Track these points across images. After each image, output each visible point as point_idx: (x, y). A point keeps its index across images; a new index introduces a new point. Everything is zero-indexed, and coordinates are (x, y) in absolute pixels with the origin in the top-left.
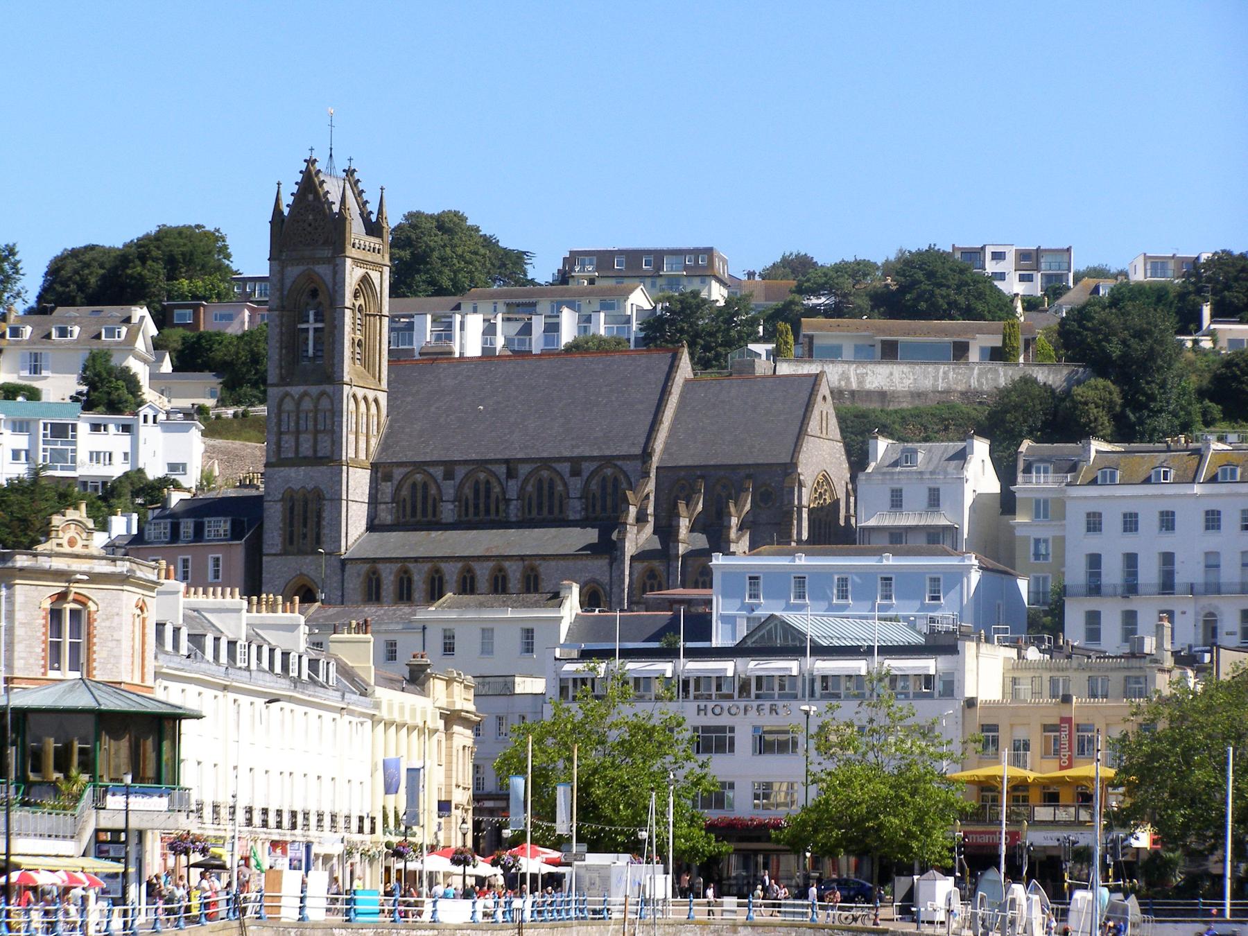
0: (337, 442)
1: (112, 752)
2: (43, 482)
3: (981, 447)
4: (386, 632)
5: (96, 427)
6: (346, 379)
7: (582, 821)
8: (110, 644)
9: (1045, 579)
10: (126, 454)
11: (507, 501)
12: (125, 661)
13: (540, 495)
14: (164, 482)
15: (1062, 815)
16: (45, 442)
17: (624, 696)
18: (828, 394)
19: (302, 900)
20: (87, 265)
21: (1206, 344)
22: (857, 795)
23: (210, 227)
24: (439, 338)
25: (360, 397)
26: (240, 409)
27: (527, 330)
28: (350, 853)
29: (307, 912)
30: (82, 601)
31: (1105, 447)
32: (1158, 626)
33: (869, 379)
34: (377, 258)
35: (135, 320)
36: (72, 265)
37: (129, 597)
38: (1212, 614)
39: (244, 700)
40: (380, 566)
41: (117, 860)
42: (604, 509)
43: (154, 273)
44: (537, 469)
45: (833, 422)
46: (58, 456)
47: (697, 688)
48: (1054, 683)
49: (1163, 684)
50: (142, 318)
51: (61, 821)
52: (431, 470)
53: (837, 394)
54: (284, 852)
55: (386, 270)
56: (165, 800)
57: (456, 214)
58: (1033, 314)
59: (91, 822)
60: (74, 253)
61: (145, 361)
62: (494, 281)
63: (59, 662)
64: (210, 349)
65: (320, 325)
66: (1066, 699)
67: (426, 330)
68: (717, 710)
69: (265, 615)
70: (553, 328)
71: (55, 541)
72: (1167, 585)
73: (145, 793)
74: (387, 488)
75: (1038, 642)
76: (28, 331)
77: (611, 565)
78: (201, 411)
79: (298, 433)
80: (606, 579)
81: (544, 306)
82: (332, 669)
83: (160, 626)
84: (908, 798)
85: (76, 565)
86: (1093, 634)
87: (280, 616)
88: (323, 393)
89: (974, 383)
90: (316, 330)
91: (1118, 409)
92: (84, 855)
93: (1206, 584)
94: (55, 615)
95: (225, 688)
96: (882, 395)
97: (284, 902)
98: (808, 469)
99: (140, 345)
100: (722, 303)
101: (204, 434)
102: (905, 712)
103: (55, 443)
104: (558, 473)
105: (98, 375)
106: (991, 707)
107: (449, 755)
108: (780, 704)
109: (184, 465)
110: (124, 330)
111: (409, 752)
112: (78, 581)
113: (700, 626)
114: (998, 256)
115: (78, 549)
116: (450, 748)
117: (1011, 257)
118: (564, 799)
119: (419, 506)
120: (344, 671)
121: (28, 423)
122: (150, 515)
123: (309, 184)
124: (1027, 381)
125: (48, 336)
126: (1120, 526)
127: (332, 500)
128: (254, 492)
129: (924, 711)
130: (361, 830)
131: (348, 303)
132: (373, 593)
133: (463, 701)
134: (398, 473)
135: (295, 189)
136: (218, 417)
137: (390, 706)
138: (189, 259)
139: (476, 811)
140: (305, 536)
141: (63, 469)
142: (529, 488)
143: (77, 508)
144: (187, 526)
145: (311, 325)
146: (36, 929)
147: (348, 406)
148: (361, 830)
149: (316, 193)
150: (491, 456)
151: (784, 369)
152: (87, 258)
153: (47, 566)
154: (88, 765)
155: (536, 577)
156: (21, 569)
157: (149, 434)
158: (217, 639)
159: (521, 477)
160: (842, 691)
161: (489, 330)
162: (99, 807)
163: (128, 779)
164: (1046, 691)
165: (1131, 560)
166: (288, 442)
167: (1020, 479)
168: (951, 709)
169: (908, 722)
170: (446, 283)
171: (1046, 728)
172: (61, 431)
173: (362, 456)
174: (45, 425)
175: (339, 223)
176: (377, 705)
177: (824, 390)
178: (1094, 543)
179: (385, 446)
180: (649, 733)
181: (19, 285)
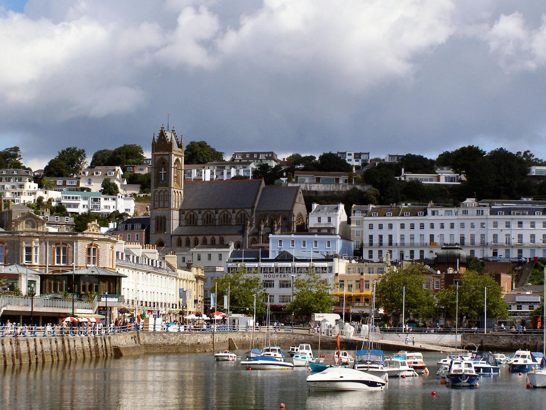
0: (170, 204)
1: (104, 286)
2: (91, 214)
3: (342, 207)
4: (182, 255)
5: (106, 199)
6: (172, 187)
7: (232, 305)
8: (104, 257)
9: (359, 241)
10: (114, 206)
11: (216, 220)
12: (108, 262)
13: (241, 217)
14: (124, 214)
15: (361, 305)
16: (92, 203)
17: (244, 272)
18: (301, 191)
19: (154, 325)
20: (104, 155)
21: (403, 179)
22: (305, 299)
23: (138, 145)
24: (198, 176)
25: (176, 191)
26: (145, 194)
27: (222, 174)
28: (170, 314)
29: (156, 329)
30: (96, 246)
31: (374, 207)
32: (387, 254)
33: (312, 188)
34: (181, 154)
35: (116, 170)
36: (100, 154)
37: (109, 245)
38: (402, 251)
39: (141, 273)
40: (181, 237)
41: (104, 315)
42: (241, 222)
43: (122, 157)
44: (224, 211)
45: (303, 199)
46: (95, 207)
47: (264, 270)
48: (359, 269)
49: (387, 270)
50: (119, 169)
51: (87, 305)
52: (195, 211)
53: (304, 191)
54: (152, 313)
55: (183, 157)
56: (117, 299)
57: (204, 142)
58: (358, 171)
59: (97, 305)
60: (101, 152)
61: (119, 181)
62: (214, 160)
63: (90, 262)
64: (137, 178)
65: (165, 172)
66: (362, 274)
67: (194, 174)
68: (269, 276)
69: (147, 250)
70: (229, 173)
71: (89, 230)
72: (390, 244)
73: (112, 297)
74: (184, 216)
75: (354, 258)
76: (87, 173)
77: (243, 237)
78: (135, 195)
79: (159, 201)
80: (242, 241)
81: (227, 167)
82: (165, 264)
83: (118, 253)
84: (319, 300)
85: (94, 236)
86: (371, 257)
87: (151, 250)
88: (166, 191)
89: (340, 189)
90: (164, 173)
91: (379, 196)
92: (95, 313)
93: (411, 243)
94: (89, 250)
95: (135, 269)
96: (316, 192)
97: (149, 326)
98: (296, 212)
99: (118, 177)
100: (274, 167)
101: (135, 201)
102: (318, 277)
103: (95, 203)
104: (212, 212)
105: (107, 185)
106: (342, 276)
107: (197, 288)
108: (286, 274)
109: (130, 209)
110: (114, 173)
111: (184, 285)
112: (95, 241)
113: (266, 253)
114: (350, 155)
115: (95, 232)
116: (197, 286)
117: (353, 155)
118: (226, 299)
119: (192, 221)
120: (169, 265)
121: (87, 198)
122: (120, 223)
123: (162, 134)
124: (355, 189)
125: (93, 174)
126: (419, 227)
127: (168, 219)
128: (148, 217)
129: (323, 276)
130: (173, 308)
131: (173, 166)
132: (179, 244)
133: (201, 273)
134: (186, 212)
135: (158, 135)
136: (139, 196)
137: (181, 274)
138: (132, 154)
139: (205, 303)
140: (161, 229)
141: (97, 210)
142: (204, 217)
143: (94, 221)
144: (129, 226)
145: (163, 172)
146: (245, 336)
147: (173, 194)
148: (173, 308)
149: (164, 136)
150: (211, 207)
151: (290, 185)
152: (104, 153)
153: (87, 236)
154: (97, 290)
155: (223, 240)
156: (79, 237)
157: (120, 200)
158: (133, 256)
159: (219, 213)
160: (303, 271)
161: (212, 174)
162: (99, 300)
163: (107, 293)
164: (357, 272)
165: (381, 237)
166: (157, 203)
167: (352, 214)
168: (332, 276)
169: (319, 279)
170: (201, 160)
171: (357, 281)
172: (96, 200)
173: (177, 207)
174: (92, 198)
175: (171, 144)
176: (177, 274)
177: (300, 191)
178: (371, 232)
179: (183, 204)
180: (251, 282)
181: (85, 161)
